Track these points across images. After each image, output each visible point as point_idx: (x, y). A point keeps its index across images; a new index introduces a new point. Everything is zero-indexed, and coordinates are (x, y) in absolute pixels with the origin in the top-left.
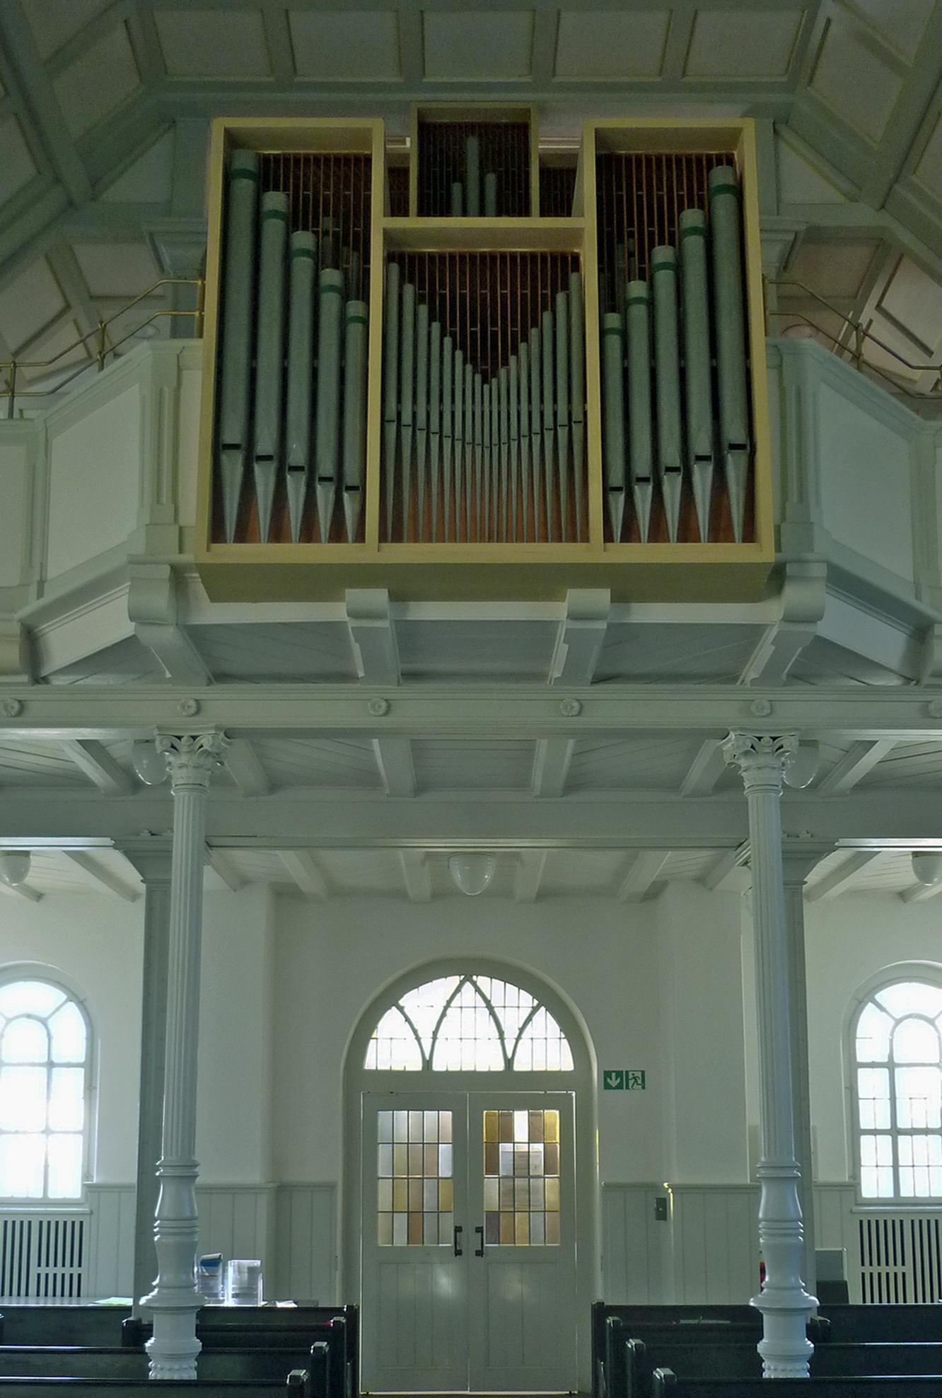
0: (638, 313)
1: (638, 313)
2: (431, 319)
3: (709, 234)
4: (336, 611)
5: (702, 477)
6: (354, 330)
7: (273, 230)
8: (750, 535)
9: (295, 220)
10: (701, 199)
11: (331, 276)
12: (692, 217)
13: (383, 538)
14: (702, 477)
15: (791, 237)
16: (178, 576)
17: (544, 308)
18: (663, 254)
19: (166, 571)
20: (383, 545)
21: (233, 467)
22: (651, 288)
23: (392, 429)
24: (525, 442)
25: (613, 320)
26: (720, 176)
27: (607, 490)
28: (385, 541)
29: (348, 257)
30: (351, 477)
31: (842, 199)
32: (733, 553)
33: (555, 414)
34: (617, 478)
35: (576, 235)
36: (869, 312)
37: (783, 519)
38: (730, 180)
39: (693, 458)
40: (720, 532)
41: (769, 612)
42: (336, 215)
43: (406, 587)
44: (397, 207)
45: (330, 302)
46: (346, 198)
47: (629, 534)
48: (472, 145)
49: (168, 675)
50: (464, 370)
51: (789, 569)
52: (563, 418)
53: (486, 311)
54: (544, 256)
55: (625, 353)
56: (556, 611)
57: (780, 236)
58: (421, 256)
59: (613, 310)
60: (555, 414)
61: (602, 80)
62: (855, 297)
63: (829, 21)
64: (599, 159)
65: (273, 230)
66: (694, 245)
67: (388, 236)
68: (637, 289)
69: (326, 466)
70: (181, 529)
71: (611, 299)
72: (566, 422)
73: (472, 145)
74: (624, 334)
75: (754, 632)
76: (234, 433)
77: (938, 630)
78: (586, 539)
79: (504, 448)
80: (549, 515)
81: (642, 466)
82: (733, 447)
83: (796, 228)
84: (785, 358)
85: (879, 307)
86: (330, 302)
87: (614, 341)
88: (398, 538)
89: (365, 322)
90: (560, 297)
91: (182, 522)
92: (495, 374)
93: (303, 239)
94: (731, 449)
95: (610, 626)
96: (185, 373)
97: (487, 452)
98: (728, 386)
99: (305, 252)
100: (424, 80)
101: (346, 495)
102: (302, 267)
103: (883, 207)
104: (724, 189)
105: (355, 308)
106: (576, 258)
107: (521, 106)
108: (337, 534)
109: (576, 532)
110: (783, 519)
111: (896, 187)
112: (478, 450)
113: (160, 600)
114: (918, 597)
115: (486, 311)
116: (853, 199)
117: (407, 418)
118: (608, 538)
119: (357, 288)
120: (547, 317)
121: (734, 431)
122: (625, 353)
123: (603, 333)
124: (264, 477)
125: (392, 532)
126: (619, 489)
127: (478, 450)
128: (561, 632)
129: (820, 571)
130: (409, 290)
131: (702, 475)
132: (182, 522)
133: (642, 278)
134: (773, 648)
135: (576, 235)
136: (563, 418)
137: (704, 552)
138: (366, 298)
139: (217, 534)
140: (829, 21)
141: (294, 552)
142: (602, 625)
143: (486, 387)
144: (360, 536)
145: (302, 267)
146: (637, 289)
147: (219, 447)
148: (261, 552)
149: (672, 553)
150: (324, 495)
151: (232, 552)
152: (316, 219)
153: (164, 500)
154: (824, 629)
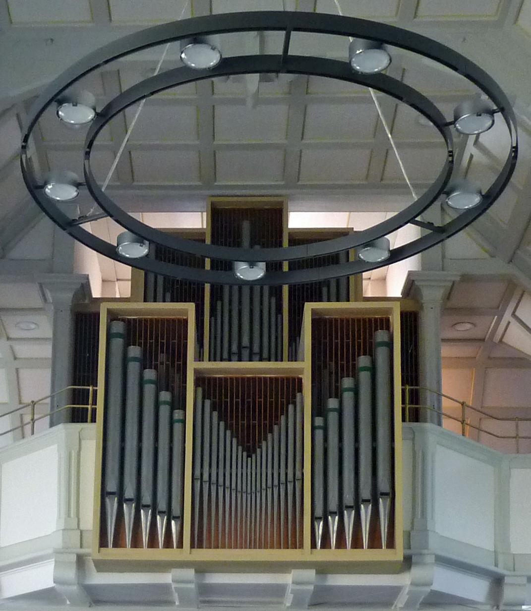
0: (333, 417)
1: (333, 417)
2: (220, 419)
3: (373, 370)
4: (166, 578)
5: (366, 512)
6: (177, 427)
7: (134, 368)
8: (391, 544)
9: (146, 362)
10: (371, 350)
11: (165, 396)
12: (363, 361)
13: (192, 546)
14: (366, 512)
15: (450, 284)
16: (81, 561)
17: (282, 414)
18: (347, 382)
19: (74, 558)
20: (193, 550)
21: (112, 505)
22: (341, 403)
23: (198, 484)
24: (269, 491)
25: (319, 421)
26: (381, 336)
27: (314, 519)
28: (194, 548)
29: (173, 377)
30: (176, 511)
31: (487, 256)
32: (382, 554)
33: (286, 474)
34: (319, 512)
35: (301, 371)
36: (507, 316)
37: (412, 528)
38: (386, 339)
39: (361, 501)
40: (374, 543)
41: (404, 580)
42: (167, 353)
43: (202, 569)
44: (199, 357)
45: (164, 411)
46: (174, 344)
47: (326, 544)
48: (246, 226)
49: (68, 602)
50: (237, 449)
51: (414, 559)
52: (290, 477)
53: (250, 413)
54: (283, 379)
55: (326, 439)
56: (287, 578)
57: (442, 284)
58: (215, 379)
59: (319, 415)
60: (286, 474)
61: (331, 183)
62: (498, 307)
63: (472, 156)
64: (313, 320)
65: (134, 368)
66: (365, 377)
67: (196, 371)
68: (333, 403)
69: (162, 505)
70: (81, 532)
71: (319, 409)
72: (292, 480)
73: (246, 226)
74: (325, 429)
75: (395, 591)
76: (112, 486)
77: (507, 580)
78: (301, 546)
79: (258, 495)
80: (282, 530)
81: (333, 505)
82: (383, 494)
83: (453, 279)
84: (416, 434)
85: (514, 314)
86: (164, 411)
87: (319, 433)
88: (200, 546)
89: (184, 422)
90: (291, 407)
91: (82, 527)
92: (255, 452)
93: (150, 374)
94: (382, 494)
95: (316, 587)
96: (83, 442)
97: (249, 496)
98: (382, 460)
99: (151, 382)
100: (214, 143)
101: (173, 522)
102: (149, 389)
103: (511, 261)
104: (383, 344)
105: (178, 414)
106: (300, 380)
107: (276, 199)
108: (168, 544)
109: (297, 544)
110: (412, 528)
111: (518, 252)
112: (244, 495)
113: (71, 574)
114: (496, 565)
115: (250, 413)
116: (492, 256)
117: (206, 477)
118: (314, 546)
119: (179, 403)
120: (283, 418)
121: (383, 486)
122: (326, 439)
123: (313, 428)
124: (128, 511)
125: (197, 542)
126: (320, 518)
127: (244, 495)
128: (289, 590)
129: (430, 559)
130: (208, 403)
131: (368, 502)
132: (82, 527)
133: (336, 397)
134: (407, 597)
135: (301, 371)
136: (290, 477)
137: (365, 554)
138: (184, 408)
139: (103, 543)
140: (472, 156)
141: (144, 553)
142: (311, 588)
143: (249, 459)
144: (180, 545)
145: (149, 389)
146: (333, 403)
147: (104, 494)
148: (127, 553)
149: (349, 555)
150: (161, 522)
151: (112, 553)
152: (156, 355)
153: (72, 515)
154: (436, 587)
